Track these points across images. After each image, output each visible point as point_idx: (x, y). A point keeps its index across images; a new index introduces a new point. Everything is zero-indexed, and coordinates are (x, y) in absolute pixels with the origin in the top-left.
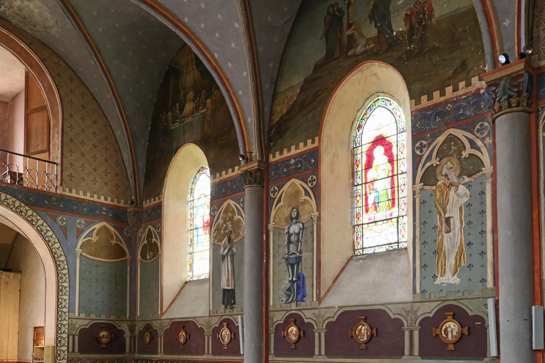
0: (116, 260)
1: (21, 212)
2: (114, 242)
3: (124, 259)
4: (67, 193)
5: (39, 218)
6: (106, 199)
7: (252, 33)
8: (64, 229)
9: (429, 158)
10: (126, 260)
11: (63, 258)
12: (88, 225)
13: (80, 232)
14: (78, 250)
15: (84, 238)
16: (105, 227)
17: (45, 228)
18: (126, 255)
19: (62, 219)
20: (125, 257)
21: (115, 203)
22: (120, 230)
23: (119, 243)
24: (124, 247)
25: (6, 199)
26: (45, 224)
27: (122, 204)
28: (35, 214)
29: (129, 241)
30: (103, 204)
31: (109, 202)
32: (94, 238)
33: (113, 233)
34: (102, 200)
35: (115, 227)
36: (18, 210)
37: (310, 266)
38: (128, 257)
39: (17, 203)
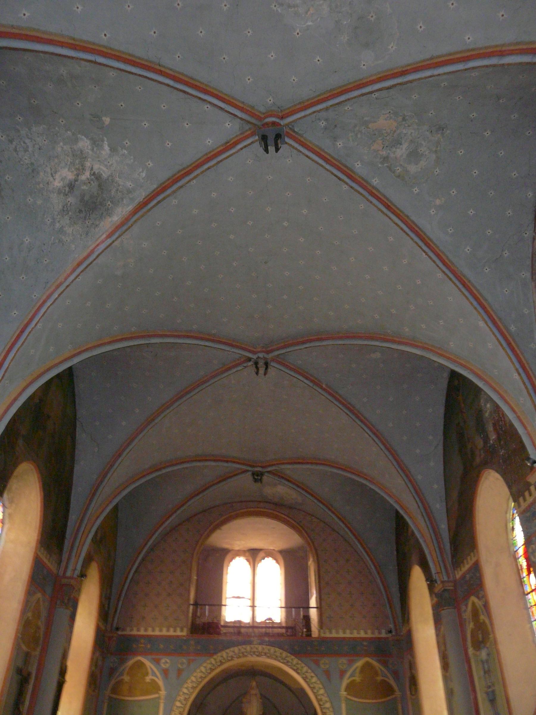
0: (383, 700)
1: (288, 662)
2: (379, 678)
3: (394, 696)
4: (328, 635)
5: (303, 665)
6: (366, 633)
7: (345, 169)
8: (327, 673)
9: (154, 674)
10: (159, 698)
11: (328, 705)
12: (351, 662)
13: (342, 673)
14: (343, 693)
15: (151, 669)
16: (367, 664)
17: (310, 674)
18: (160, 690)
19: (325, 662)
20: (158, 693)
21: (377, 635)
22: (385, 664)
23: (386, 679)
24: (392, 682)
25: (263, 649)
26: (310, 671)
27: (384, 635)
28: (300, 662)
29: (396, 674)
30: (363, 639)
31: (369, 635)
32: (357, 678)
33: (379, 671)
34: (362, 634)
35: (379, 661)
36: (285, 661)
37: (384, 93)
38: (398, 694)
39: (285, 654)
